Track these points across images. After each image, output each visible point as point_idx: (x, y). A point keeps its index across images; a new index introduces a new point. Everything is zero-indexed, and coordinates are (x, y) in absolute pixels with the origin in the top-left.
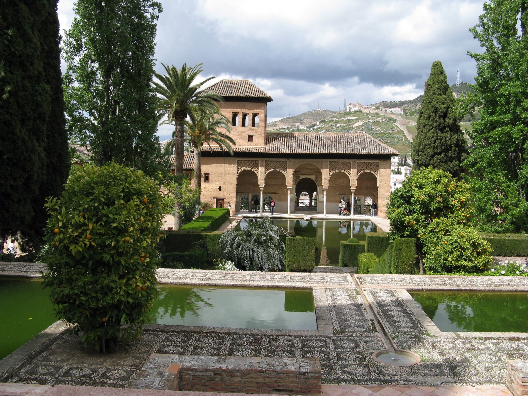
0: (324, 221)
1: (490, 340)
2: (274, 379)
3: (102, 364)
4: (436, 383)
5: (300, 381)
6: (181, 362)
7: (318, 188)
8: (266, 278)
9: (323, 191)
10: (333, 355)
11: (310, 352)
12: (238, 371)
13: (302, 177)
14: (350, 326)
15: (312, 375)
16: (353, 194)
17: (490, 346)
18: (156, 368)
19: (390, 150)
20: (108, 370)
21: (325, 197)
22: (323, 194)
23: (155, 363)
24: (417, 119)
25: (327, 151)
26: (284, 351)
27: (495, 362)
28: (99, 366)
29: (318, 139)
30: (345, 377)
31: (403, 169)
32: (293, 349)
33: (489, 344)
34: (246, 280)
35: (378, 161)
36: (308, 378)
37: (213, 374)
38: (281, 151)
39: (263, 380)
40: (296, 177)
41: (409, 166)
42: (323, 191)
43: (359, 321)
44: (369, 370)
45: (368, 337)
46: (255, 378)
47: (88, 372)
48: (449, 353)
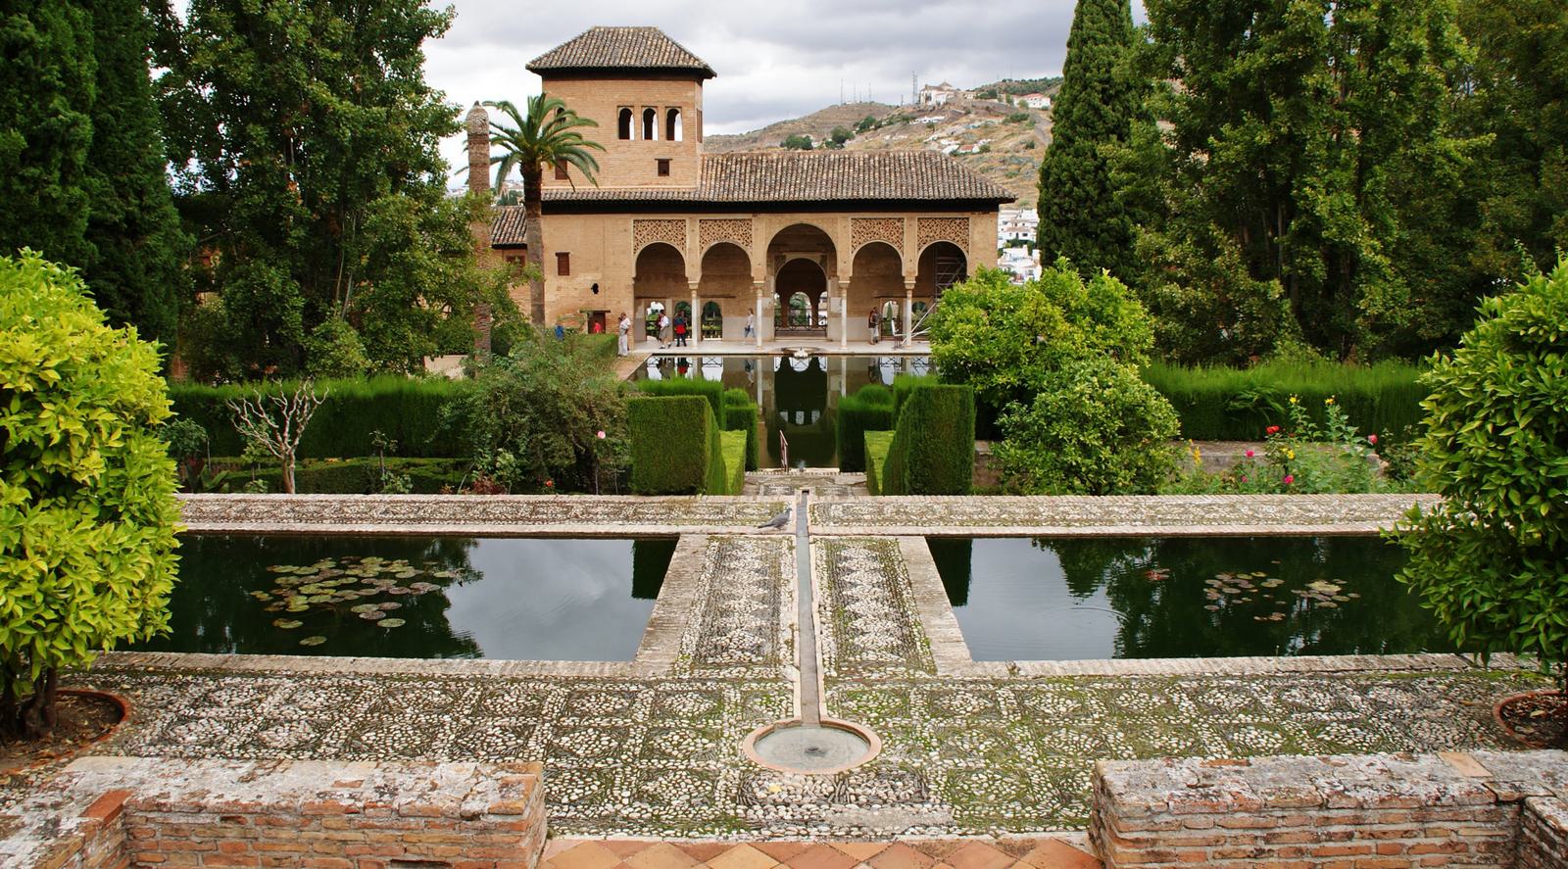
0: (844, 360)
2: (390, 832)
5: (462, 839)
7: (829, 283)
9: (840, 288)
12: (286, 809)
13: (790, 257)
15: (499, 819)
16: (910, 294)
21: (844, 302)
22: (840, 296)
25: (845, 194)
35: (966, 215)
36: (485, 830)
37: (218, 819)
40: (777, 258)
42: (840, 288)
46: (337, 829)
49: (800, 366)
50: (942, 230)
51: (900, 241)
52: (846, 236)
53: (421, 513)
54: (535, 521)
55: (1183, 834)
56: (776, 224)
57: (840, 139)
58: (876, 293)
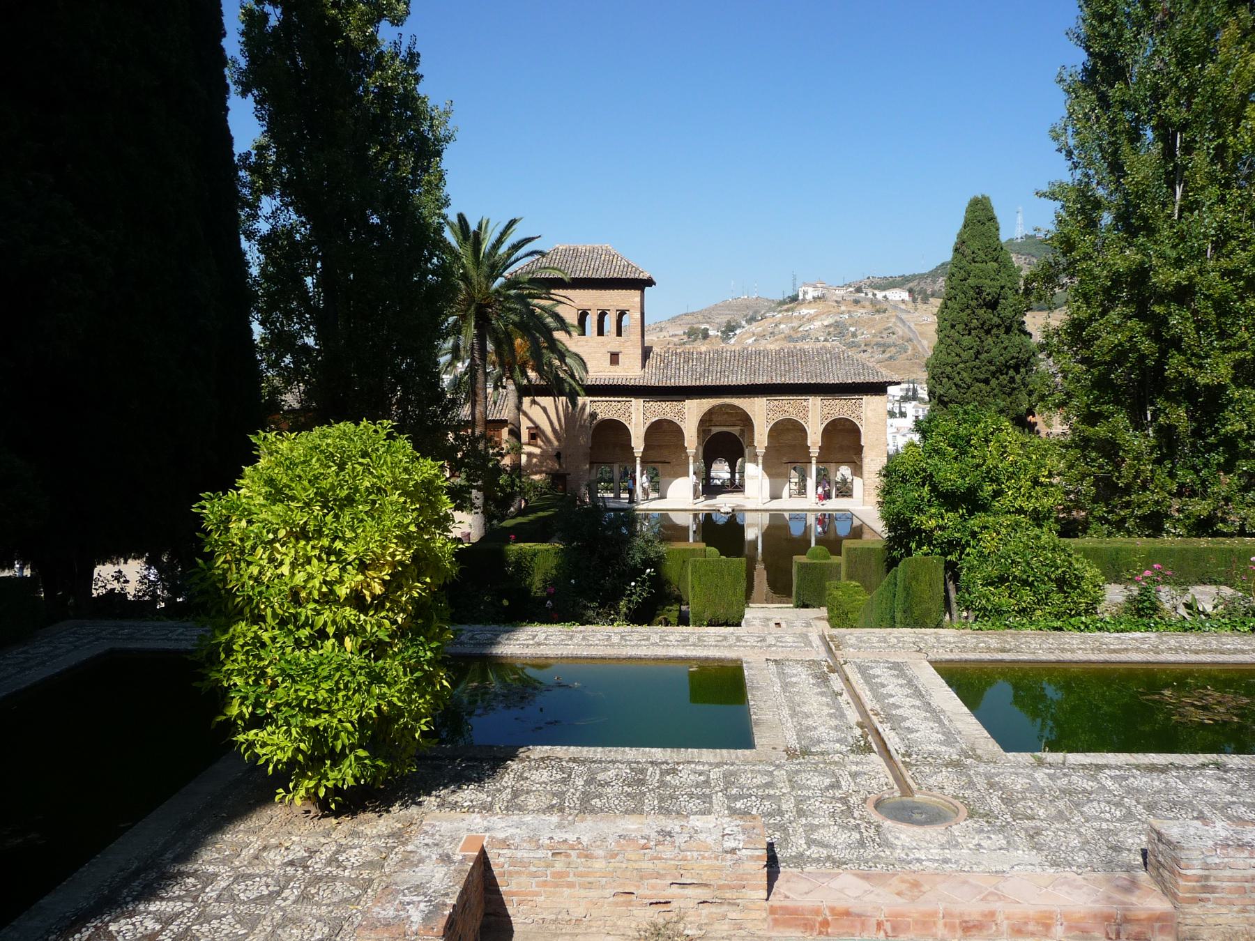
1: (1107, 771)
3: (329, 835)
4: (999, 868)
6: (487, 829)
7: (747, 451)
8: (652, 640)
10: (788, 805)
11: (741, 797)
13: (715, 430)
14: (820, 741)
17: (1109, 783)
18: (437, 845)
19: (885, 375)
20: (341, 849)
23: (433, 835)
24: (936, 310)
25: (762, 380)
26: (691, 796)
27: (1119, 820)
28: (323, 840)
29: (745, 356)
30: (814, 852)
31: (909, 408)
32: (708, 791)
33: (1105, 778)
34: (612, 645)
37: (550, 854)
38: (672, 382)
39: (650, 865)
40: (704, 431)
41: (921, 400)
43: (836, 728)
44: (861, 836)
45: (857, 764)
47: (299, 855)
48: (1023, 799)
49: (721, 520)
50: (840, 408)
51: (805, 417)
52: (762, 414)
53: (536, 639)
54: (626, 646)
55: (1228, 873)
56: (707, 403)
57: (730, 329)
58: (785, 460)
